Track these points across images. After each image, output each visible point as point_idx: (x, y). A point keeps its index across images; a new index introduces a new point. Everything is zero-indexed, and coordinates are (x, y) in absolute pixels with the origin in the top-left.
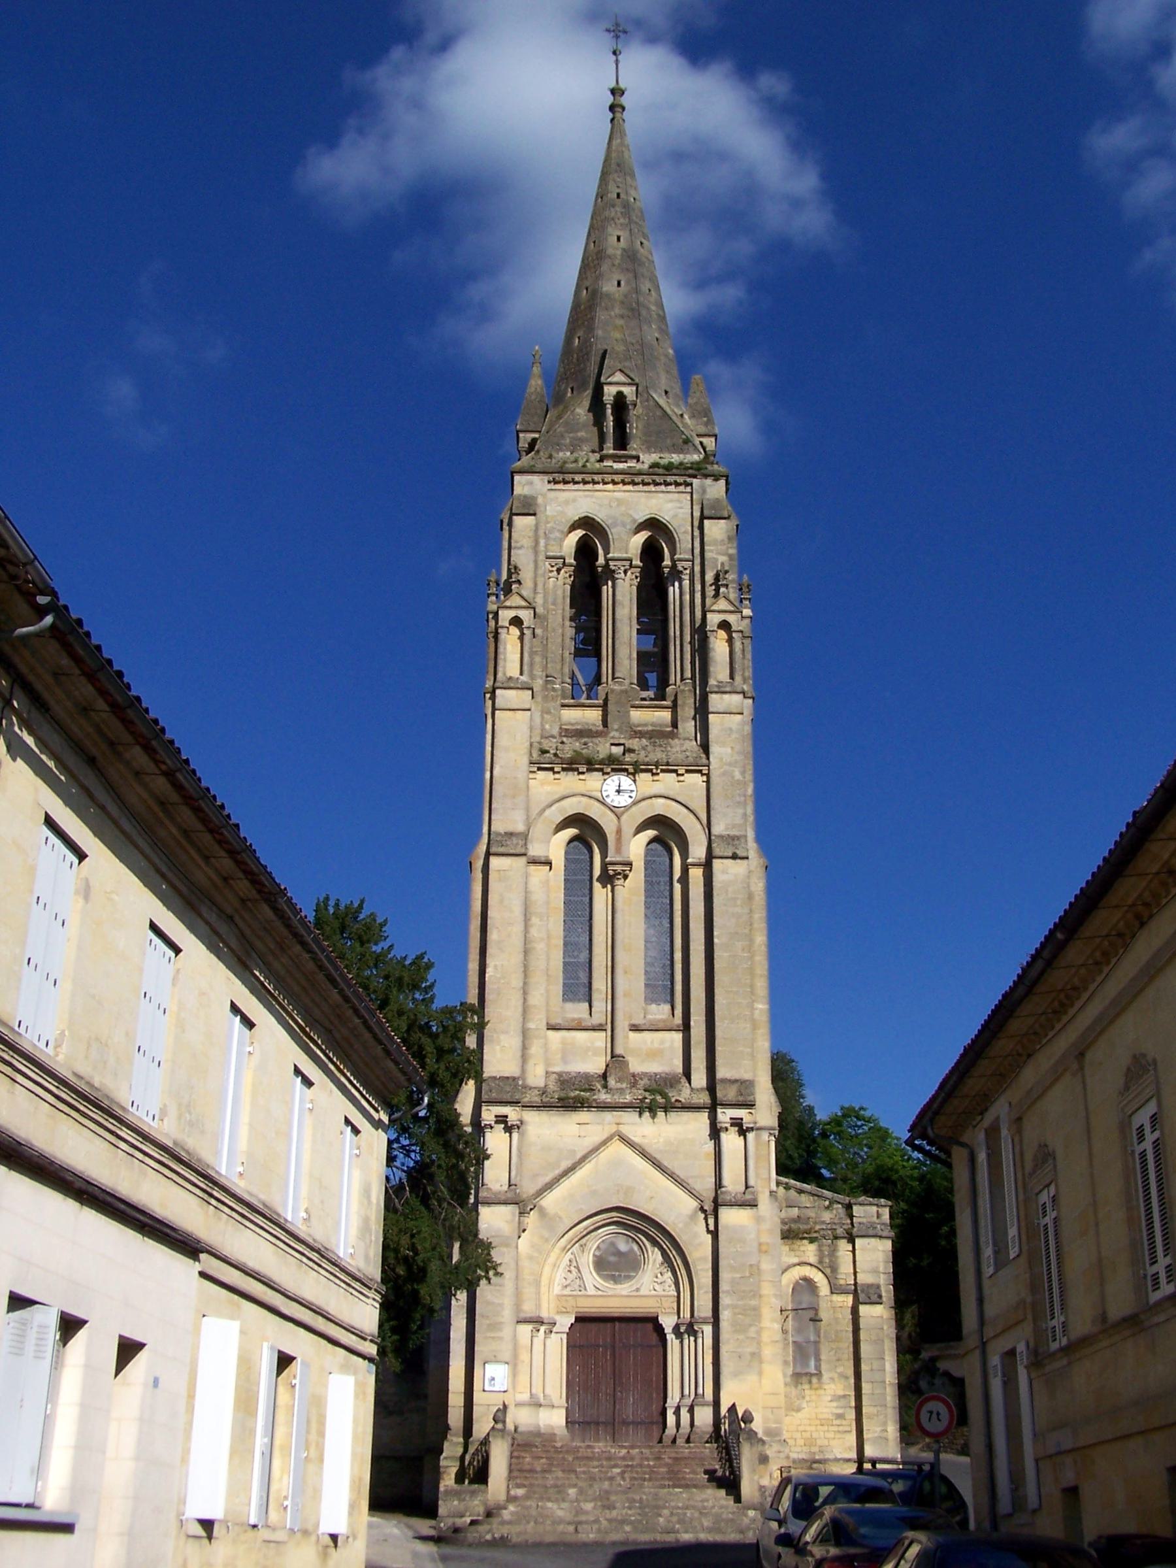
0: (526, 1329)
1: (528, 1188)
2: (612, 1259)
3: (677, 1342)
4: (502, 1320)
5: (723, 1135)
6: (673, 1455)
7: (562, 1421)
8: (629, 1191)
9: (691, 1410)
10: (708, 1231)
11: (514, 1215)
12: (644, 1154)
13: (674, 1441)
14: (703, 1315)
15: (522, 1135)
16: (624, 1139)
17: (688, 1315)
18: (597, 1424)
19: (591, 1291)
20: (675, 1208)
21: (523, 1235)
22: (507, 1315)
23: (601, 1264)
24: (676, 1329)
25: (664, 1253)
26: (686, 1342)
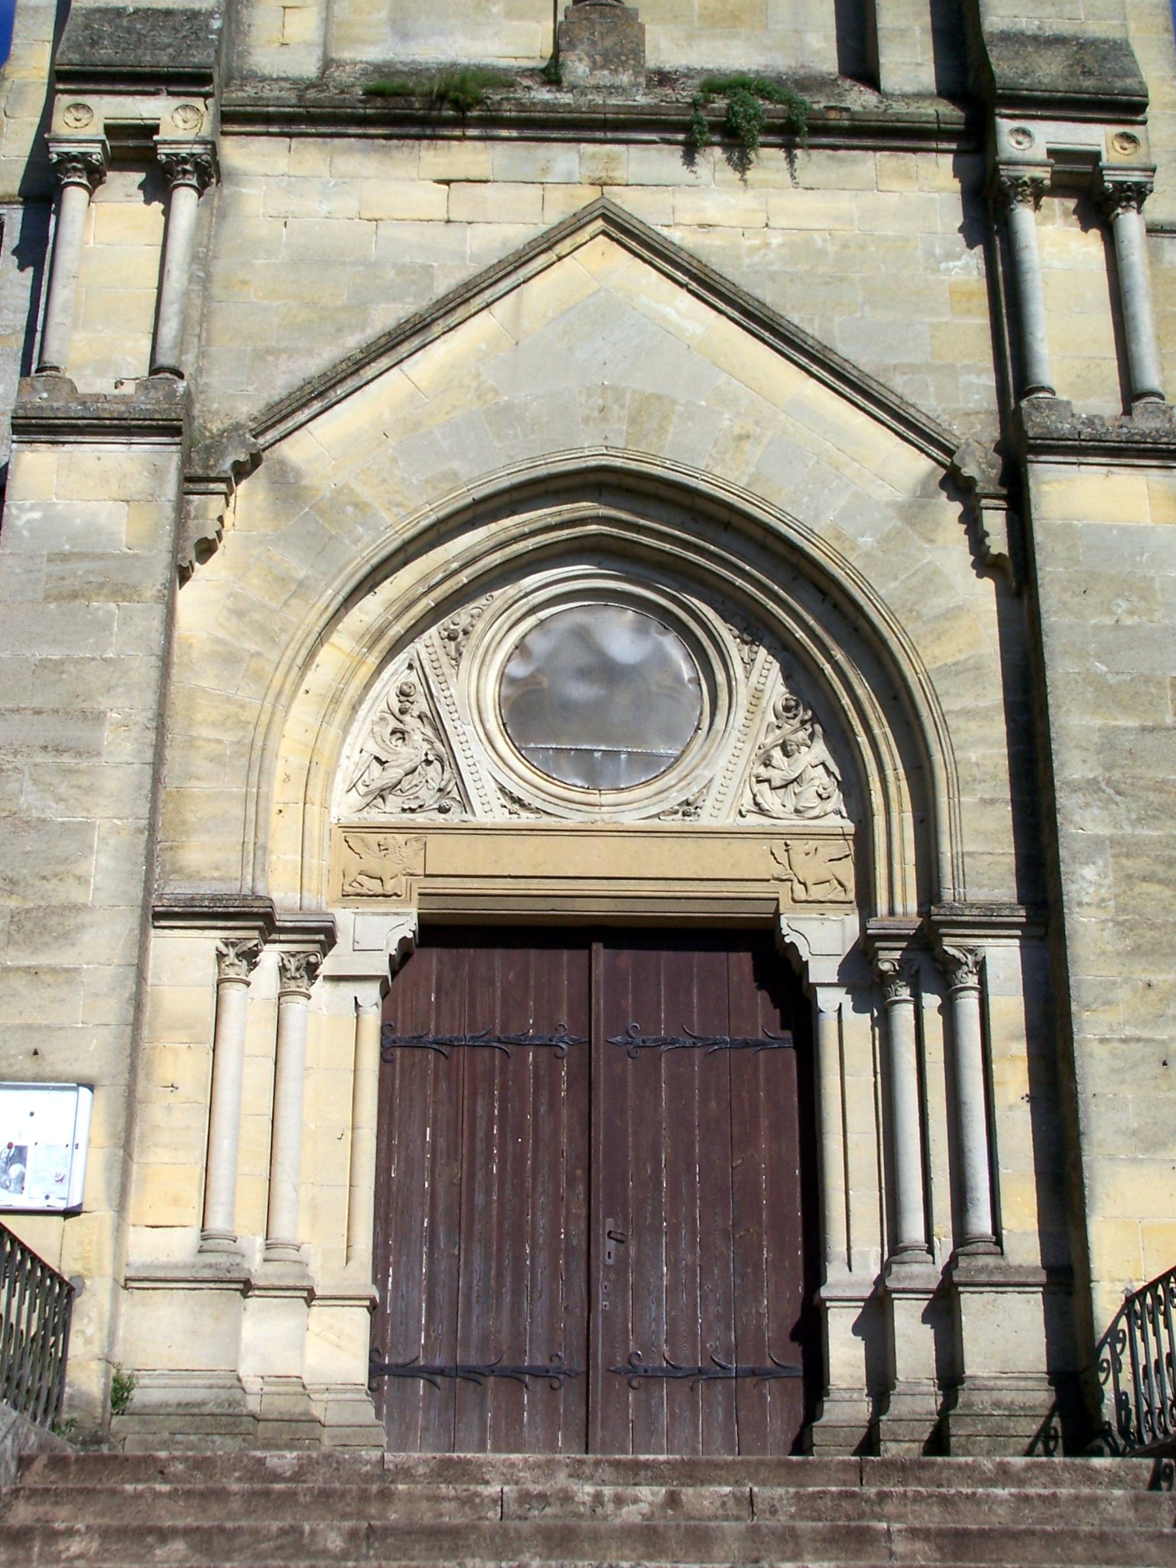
0: (187, 954)
1: (230, 396)
2: (580, 691)
3: (859, 1026)
4: (77, 895)
5: (1025, 216)
6: (933, 1517)
7: (354, 1365)
8: (649, 409)
9: (943, 1311)
10: (984, 563)
11: (157, 472)
12: (706, 284)
13: (870, 1443)
14: (977, 894)
15: (214, 219)
16: (625, 232)
17: (908, 903)
18: (515, 1376)
19: (490, 810)
20: (846, 486)
21: (201, 571)
22: (104, 874)
23: (527, 711)
24: (864, 977)
25: (798, 670)
26: (904, 1015)
